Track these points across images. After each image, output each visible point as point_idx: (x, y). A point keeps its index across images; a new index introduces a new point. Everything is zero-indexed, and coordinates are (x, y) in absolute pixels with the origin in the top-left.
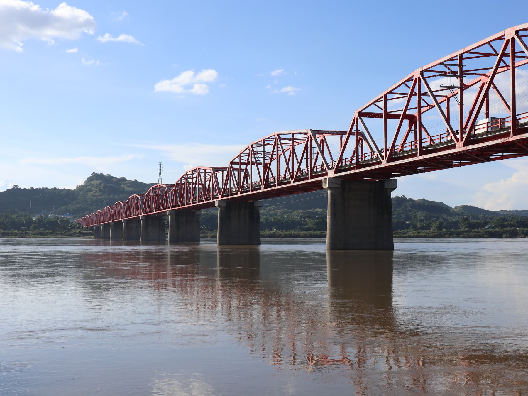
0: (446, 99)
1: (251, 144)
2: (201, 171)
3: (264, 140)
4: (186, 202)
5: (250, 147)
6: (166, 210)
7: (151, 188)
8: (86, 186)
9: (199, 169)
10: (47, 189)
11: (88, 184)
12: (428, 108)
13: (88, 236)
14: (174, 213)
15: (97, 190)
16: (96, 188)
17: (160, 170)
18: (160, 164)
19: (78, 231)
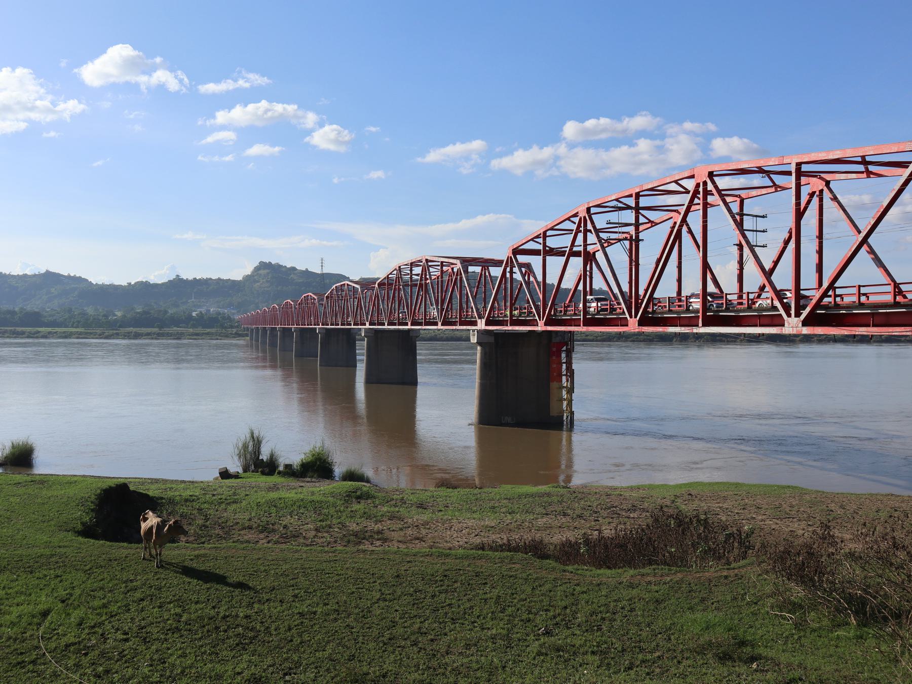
0: (738, 199)
1: (586, 207)
2: (430, 264)
3: (638, 195)
4: (361, 321)
5: (583, 214)
6: (360, 327)
7: (334, 286)
8: (253, 276)
9: (427, 261)
10: (211, 279)
11: (255, 274)
12: (649, 225)
13: (243, 337)
14: (282, 329)
15: (265, 280)
16: (263, 279)
17: (322, 266)
18: (322, 260)
19: (234, 330)
